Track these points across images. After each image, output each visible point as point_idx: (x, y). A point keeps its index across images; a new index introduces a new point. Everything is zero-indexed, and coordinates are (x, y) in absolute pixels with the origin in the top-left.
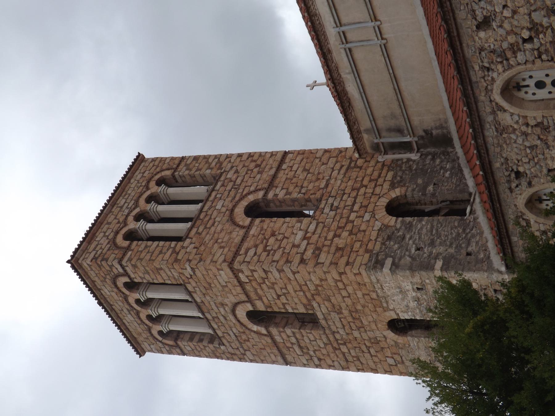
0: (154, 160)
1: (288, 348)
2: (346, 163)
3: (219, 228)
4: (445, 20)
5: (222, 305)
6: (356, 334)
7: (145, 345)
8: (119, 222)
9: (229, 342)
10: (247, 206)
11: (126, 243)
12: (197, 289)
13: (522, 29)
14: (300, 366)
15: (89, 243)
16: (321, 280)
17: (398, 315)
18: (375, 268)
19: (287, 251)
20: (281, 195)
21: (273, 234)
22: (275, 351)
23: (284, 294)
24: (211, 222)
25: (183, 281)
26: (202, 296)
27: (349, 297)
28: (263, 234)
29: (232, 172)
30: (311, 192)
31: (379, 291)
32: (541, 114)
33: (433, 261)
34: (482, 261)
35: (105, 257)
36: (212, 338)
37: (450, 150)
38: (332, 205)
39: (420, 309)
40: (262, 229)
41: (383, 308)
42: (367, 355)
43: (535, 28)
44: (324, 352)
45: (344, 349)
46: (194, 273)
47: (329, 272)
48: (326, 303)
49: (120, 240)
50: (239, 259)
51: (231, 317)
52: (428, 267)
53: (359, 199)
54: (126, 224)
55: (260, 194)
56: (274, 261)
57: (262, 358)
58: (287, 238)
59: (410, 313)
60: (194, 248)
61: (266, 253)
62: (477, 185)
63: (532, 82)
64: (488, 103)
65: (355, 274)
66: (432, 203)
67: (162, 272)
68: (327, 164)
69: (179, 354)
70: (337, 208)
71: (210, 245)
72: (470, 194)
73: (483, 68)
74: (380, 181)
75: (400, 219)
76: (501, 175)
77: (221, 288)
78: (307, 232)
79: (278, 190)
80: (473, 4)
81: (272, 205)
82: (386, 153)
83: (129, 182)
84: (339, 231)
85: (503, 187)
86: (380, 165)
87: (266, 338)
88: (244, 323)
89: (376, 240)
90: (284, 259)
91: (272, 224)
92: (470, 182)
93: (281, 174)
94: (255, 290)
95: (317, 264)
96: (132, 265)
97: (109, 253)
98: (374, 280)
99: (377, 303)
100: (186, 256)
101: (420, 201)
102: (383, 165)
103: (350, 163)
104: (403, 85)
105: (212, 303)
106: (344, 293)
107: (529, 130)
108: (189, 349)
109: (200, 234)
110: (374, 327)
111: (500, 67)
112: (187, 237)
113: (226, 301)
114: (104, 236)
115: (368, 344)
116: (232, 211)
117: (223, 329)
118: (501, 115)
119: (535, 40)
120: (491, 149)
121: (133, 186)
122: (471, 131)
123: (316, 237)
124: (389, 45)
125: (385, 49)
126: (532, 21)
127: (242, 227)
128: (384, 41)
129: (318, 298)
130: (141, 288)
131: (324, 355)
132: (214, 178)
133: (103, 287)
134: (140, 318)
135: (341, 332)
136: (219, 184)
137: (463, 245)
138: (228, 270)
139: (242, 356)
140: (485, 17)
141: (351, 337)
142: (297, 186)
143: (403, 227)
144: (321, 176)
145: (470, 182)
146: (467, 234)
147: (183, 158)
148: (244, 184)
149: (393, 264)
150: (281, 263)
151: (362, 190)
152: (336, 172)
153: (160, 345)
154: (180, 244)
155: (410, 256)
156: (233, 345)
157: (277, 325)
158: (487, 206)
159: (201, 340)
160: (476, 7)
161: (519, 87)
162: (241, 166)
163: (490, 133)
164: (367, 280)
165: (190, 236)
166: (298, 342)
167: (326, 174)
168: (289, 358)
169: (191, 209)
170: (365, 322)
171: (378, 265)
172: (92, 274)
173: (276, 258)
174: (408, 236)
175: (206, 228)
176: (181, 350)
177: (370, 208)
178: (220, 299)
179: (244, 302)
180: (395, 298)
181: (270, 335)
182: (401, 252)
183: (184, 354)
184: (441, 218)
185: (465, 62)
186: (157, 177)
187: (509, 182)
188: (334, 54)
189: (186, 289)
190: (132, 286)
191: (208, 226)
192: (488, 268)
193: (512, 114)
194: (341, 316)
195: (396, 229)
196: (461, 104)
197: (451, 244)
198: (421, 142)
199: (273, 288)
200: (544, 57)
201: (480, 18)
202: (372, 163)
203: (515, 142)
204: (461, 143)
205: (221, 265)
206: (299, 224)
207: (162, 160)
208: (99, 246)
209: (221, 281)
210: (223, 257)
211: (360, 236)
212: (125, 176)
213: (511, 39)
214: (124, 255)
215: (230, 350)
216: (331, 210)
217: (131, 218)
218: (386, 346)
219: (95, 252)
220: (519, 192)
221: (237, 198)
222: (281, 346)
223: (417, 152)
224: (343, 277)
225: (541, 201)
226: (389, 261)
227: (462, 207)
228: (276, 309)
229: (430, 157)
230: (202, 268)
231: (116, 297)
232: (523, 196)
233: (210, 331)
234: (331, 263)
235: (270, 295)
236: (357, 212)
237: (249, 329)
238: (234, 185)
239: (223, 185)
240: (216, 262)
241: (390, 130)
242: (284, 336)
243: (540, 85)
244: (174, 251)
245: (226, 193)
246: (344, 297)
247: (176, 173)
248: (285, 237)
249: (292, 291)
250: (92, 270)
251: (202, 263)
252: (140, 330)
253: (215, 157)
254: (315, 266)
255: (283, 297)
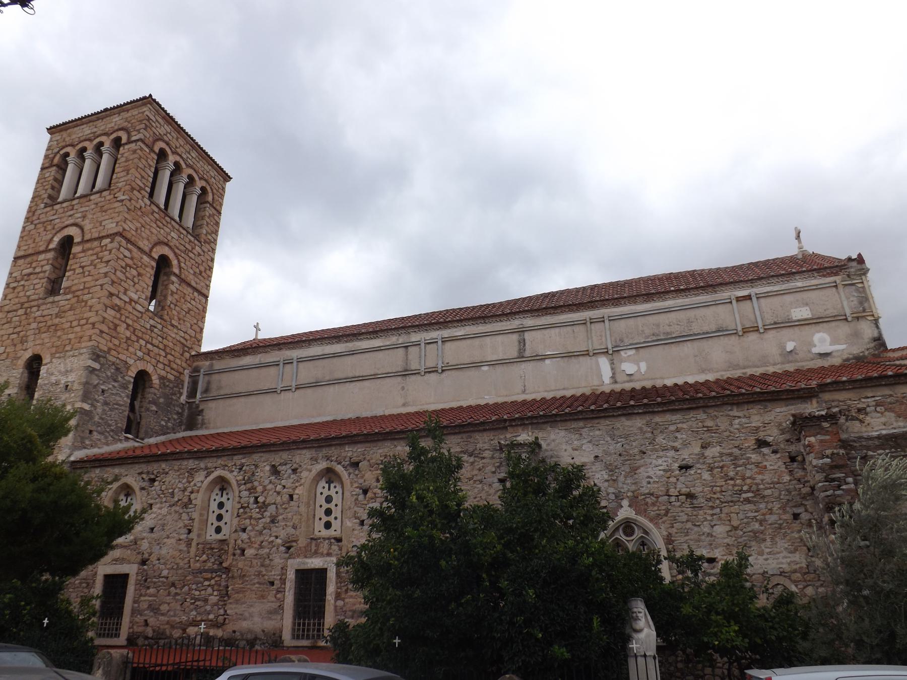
0: (223, 189)
1: (31, 263)
2: (188, 344)
3: (154, 231)
4: (283, 443)
5: (84, 217)
6: (34, 325)
7: (57, 137)
8: (176, 147)
9: (47, 213)
10: (168, 258)
11: (157, 150)
12: (103, 199)
13: (266, 498)
14: (11, 269)
15: (163, 118)
16: (91, 307)
17: (46, 364)
18: (94, 353)
19: (123, 283)
20: (172, 287)
21: (139, 275)
22: (30, 251)
23: (84, 272)
24: (160, 225)
25: (113, 190)
26: (95, 201)
27: (71, 327)
28: (141, 267)
29: (200, 251)
30: (170, 312)
31: (71, 353)
32: (198, 503)
33: (90, 402)
34: (83, 442)
35: (148, 129)
36: (53, 200)
37: (183, 427)
38: (156, 327)
39: (47, 384)
40: (146, 266)
41: (55, 354)
42: (11, 331)
43: (264, 506)
44: (22, 294)
45: (21, 312)
46: (118, 201)
47: (97, 315)
48: (69, 306)
49: (161, 144)
50: (124, 242)
51: (71, 221)
52: (85, 398)
53: (156, 350)
54: (173, 153)
55: (176, 271)
56: (115, 271)
57: (24, 239)
58: (134, 286)
59: (45, 375)
60: (141, 207)
61: (124, 266)
62: (150, 446)
63: (224, 499)
64: (214, 466)
65: (90, 336)
66: (141, 407)
67: (124, 173)
68: (191, 328)
69: (43, 164)
70: (152, 331)
71: (141, 220)
72: (143, 439)
73: (242, 465)
74: (168, 369)
75: (132, 380)
76: (155, 467)
77: (100, 220)
78: (136, 303)
79: (177, 285)
80: (291, 465)
81: (165, 278)
82: (190, 376)
83: (209, 164)
84: (132, 329)
85: (144, 468)
86: (181, 370)
87: (45, 246)
88: (62, 231)
89: (118, 358)
90: (116, 280)
91: (148, 275)
92: (152, 441)
93: (190, 290)
94: (93, 249)
95: (106, 307)
96: (136, 150)
97: (151, 133)
98: (82, 351)
99: (60, 350)
100: (134, 198)
101: (145, 398)
102: (181, 373)
103: (188, 347)
104: (242, 400)
105: (87, 208)
106: (75, 323)
107: (187, 493)
108: (47, 175)
109: (152, 214)
110: (38, 342)
111: (241, 478)
112: (152, 202)
113: (87, 221)
114: (167, 132)
115: (22, 334)
116: (167, 245)
117: (61, 211)
118: (203, 473)
119: (255, 506)
120: (178, 463)
121: (205, 167)
122: (196, 450)
123: (131, 310)
124: (275, 395)
125: (273, 391)
126: (269, 505)
127: (151, 250)
128: (279, 392)
129: (74, 300)
130: (113, 151)
131: (18, 293)
132: (198, 235)
133: (121, 117)
134: (85, 140)
135: (38, 313)
136: (192, 239)
137: (99, 428)
138: (115, 231)
139: (30, 220)
140: (279, 472)
141: (31, 320)
142: (177, 301)
143: (124, 382)
144: (181, 322)
145: (152, 441)
146: (108, 432)
147: (220, 213)
148: (187, 258)
149: (94, 369)
150: (113, 277)
151: (163, 353)
152: (183, 335)
153: (56, 150)
154: (147, 195)
155: (98, 384)
156: (43, 216)
157: (55, 259)
158: (130, 453)
159: (53, 188)
160: (288, 466)
161: (222, 489)
162: (203, 259)
163: (191, 464)
164: (83, 345)
165: (152, 205)
166: (35, 273)
167: (182, 326)
168: (21, 262)
169: (175, 211)
170: (44, 335)
171: (95, 357)
172: (135, 112)
173: (118, 273)
174: (116, 384)
175: (157, 220)
176: (47, 168)
177: (147, 358)
178: (90, 216)
179: (83, 236)
180: (62, 365)
181: (47, 251)
182: (103, 377)
183: (43, 169)
184: (126, 413)
185: (249, 453)
186: (208, 188)
187: (148, 473)
188: (277, 352)
189: (105, 190)
190: (117, 143)
191: (158, 222)
192: (75, 446)
193: (202, 482)
194: (54, 316)
195: (124, 376)
196: (218, 445)
197: (102, 419)
198: (194, 406)
199: (91, 265)
200: (241, 510)
201: (279, 468)
202: (184, 365)
203: (180, 482)
204: (187, 437)
205: (121, 226)
206: (144, 297)
207: (222, 196)
208: (159, 125)
209: (107, 222)
210: (128, 229)
211: (124, 346)
212: (215, 163)
213: (260, 489)
214: (147, 145)
215: (39, 212)
216: (151, 326)
217: (178, 158)
218: (17, 349)
219: (154, 120)
220: (137, 479)
221: (177, 251)
222: (35, 258)
223: (187, 402)
224: (91, 326)
225: (127, 495)
226: (97, 366)
227: (133, 431)
228: (70, 262)
229: (180, 411)
230: (121, 209)
231: (109, 126)
232: (134, 482)
233: (60, 200)
234: (104, 318)
235: (85, 261)
236: (145, 346)
237: (56, 234)
238: (189, 251)
239: (190, 241)
240: (125, 222)
241: (209, 383)
242: (42, 263)
243: (221, 505)
244: (141, 188)
245: (183, 243)
246: (71, 322)
247: (208, 205)
248: (135, 284)
249: (85, 279)
250: (139, 113)
251: (126, 210)
252: (74, 137)
253: (215, 240)
254: (105, 305)
255: (81, 271)
